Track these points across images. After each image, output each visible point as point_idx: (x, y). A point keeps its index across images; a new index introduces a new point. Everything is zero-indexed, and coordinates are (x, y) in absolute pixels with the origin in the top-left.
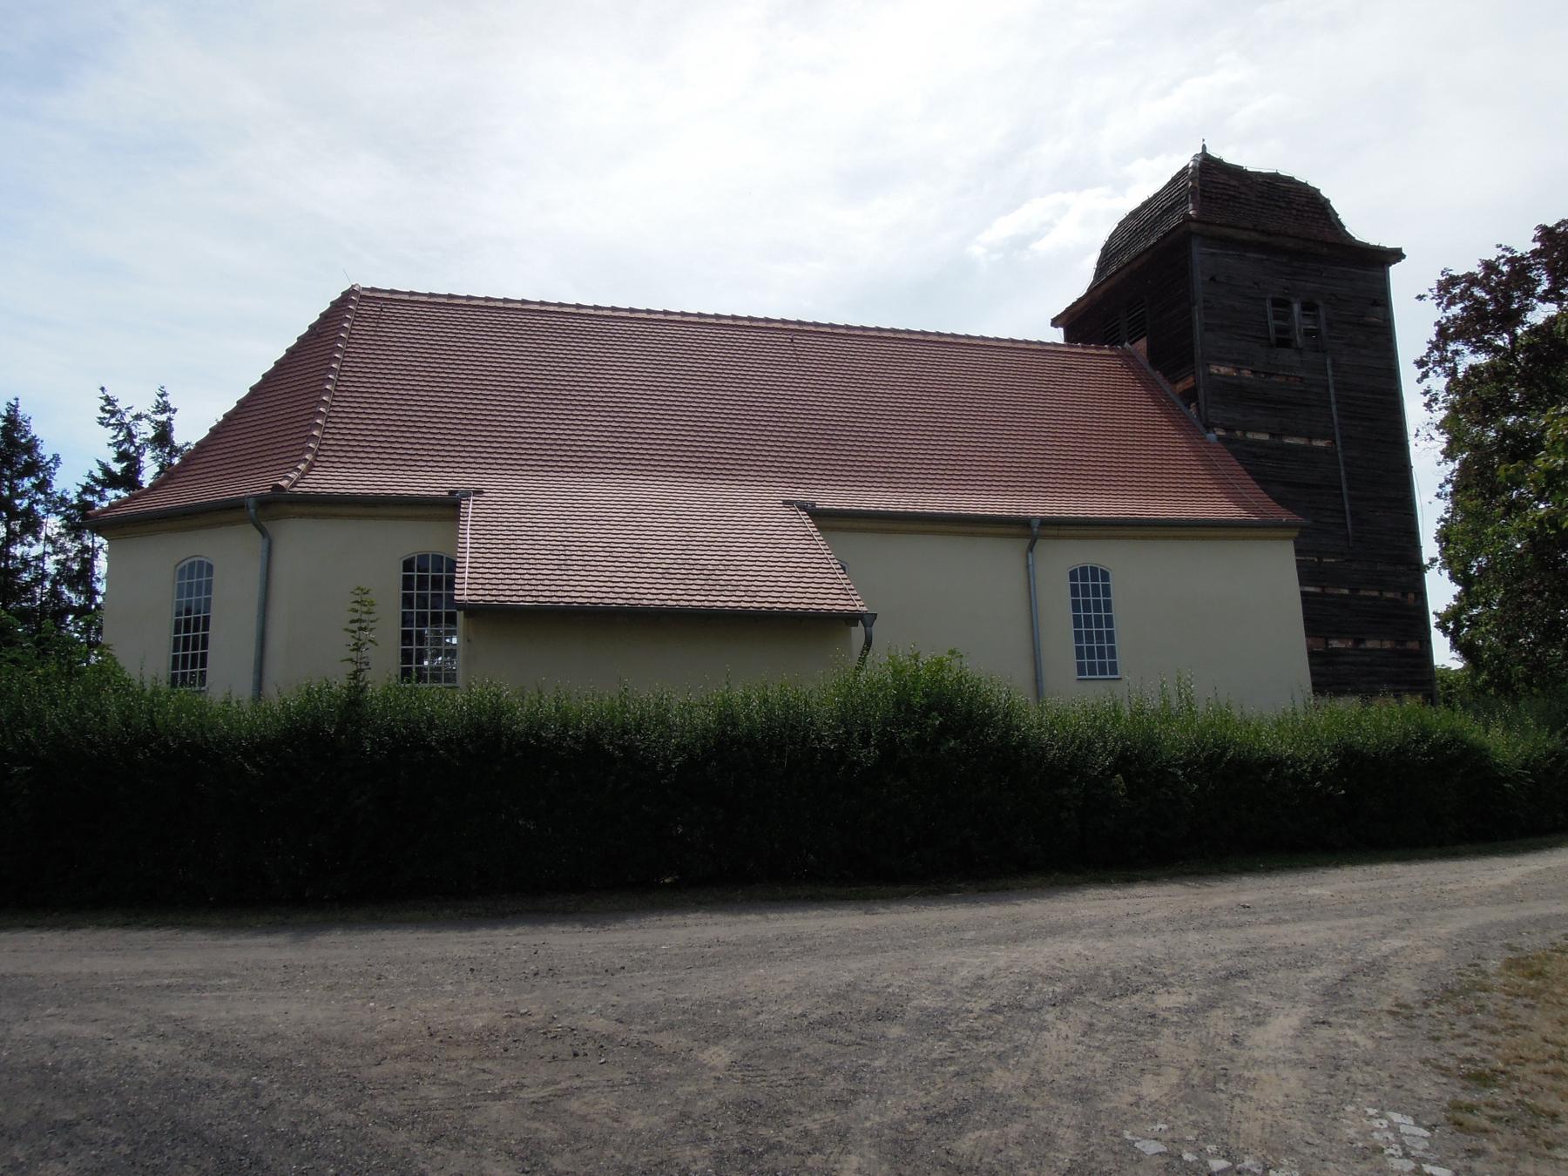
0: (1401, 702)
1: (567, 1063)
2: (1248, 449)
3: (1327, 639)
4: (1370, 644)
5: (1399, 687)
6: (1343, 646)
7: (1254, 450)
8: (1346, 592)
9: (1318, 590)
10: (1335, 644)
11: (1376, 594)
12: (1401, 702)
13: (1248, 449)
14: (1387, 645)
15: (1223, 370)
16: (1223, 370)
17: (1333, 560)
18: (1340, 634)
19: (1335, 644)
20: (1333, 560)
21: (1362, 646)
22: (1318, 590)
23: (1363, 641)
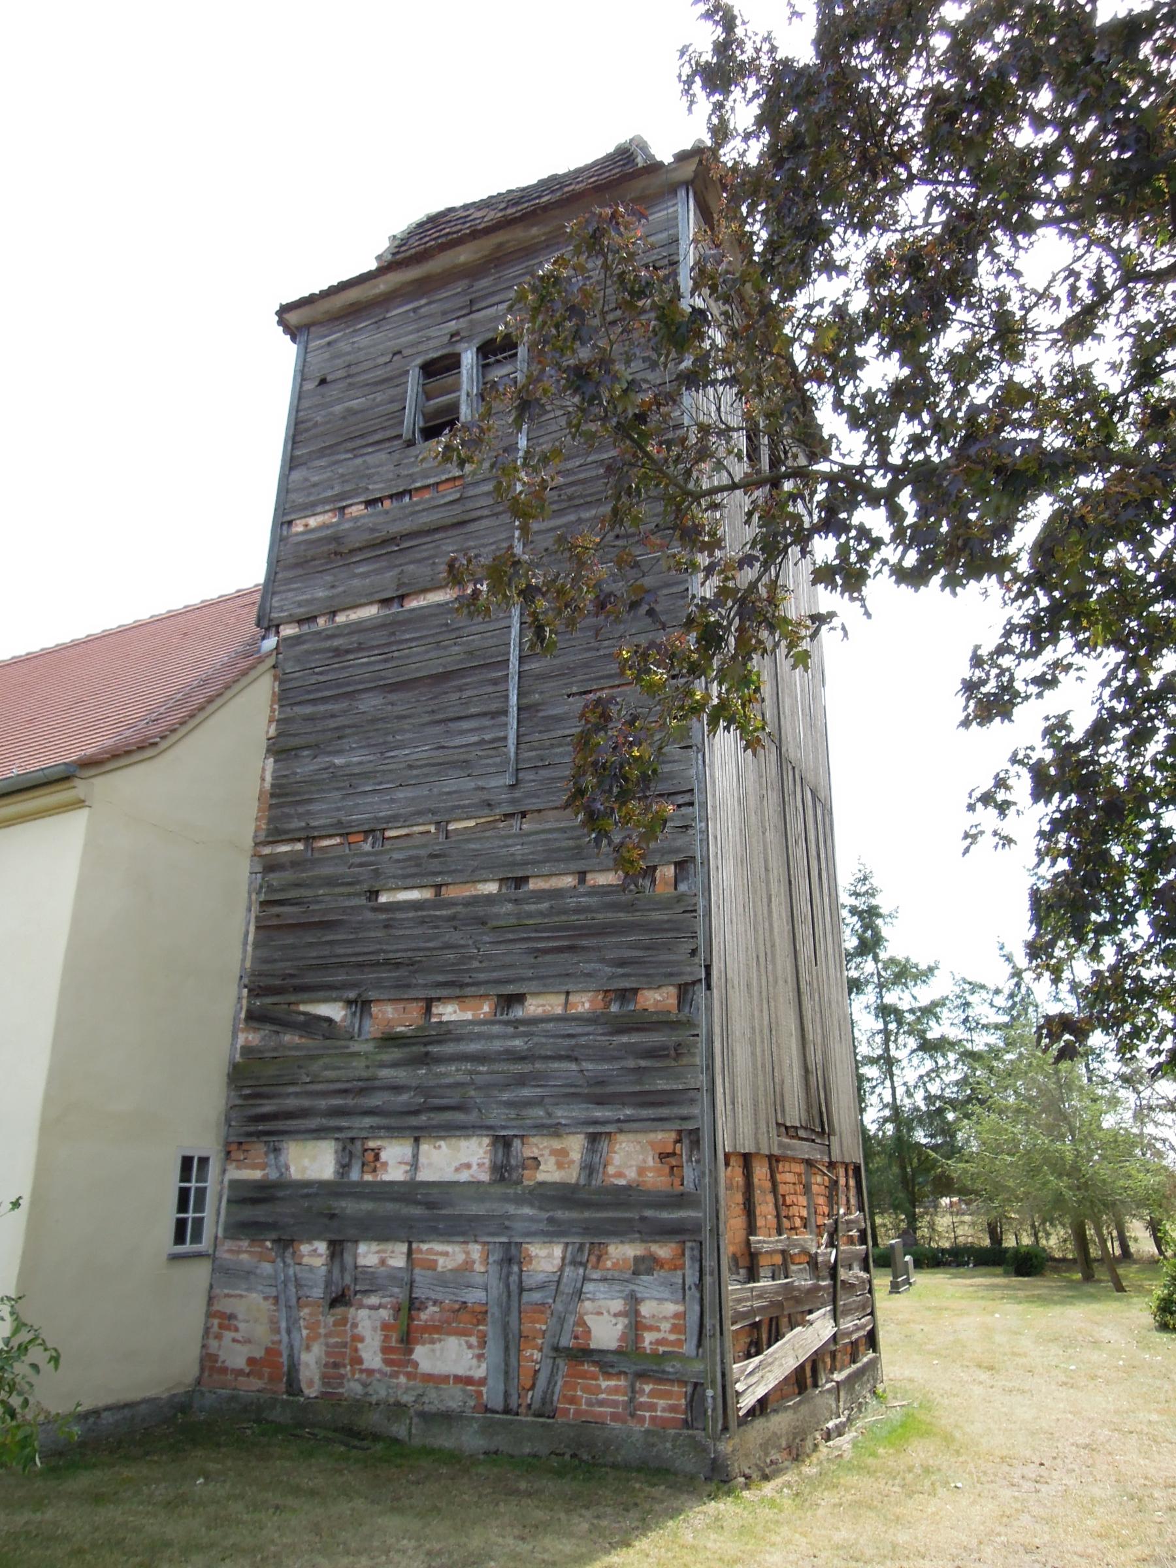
0: (1099, 337)
1: (1079, 1549)
2: (328, 644)
3: (429, 1002)
4: (534, 1007)
5: (599, 1113)
6: (468, 1016)
7: (336, 643)
8: (492, 888)
9: (428, 894)
10: (448, 1012)
11: (569, 881)
12: (1099, 337)
13: (328, 644)
14: (583, 1003)
15: (313, 522)
16: (313, 522)
17: (472, 823)
18: (458, 989)
19: (448, 1012)
20: (472, 823)
21: (518, 1013)
22: (428, 894)
23: (519, 998)
